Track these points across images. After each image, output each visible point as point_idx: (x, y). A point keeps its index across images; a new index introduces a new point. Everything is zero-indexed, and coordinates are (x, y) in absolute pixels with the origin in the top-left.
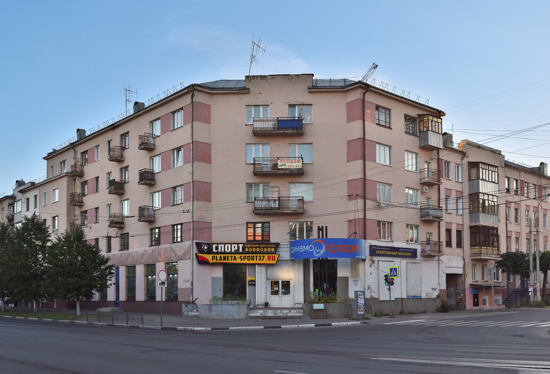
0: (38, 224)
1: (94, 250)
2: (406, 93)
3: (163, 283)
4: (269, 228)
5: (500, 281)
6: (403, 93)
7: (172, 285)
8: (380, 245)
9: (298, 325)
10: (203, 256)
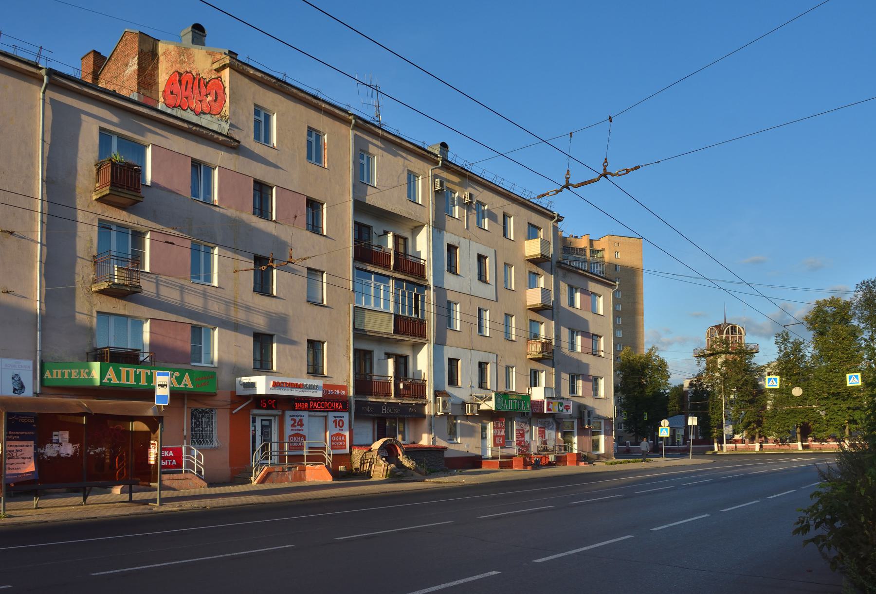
0: (840, 463)
1: (665, 423)
2: (499, 180)
3: (574, 443)
4: (355, 442)
5: (215, 443)
6: (524, 193)
7: (787, 392)
8: (267, 72)
9: (734, 445)
10: (576, 313)
